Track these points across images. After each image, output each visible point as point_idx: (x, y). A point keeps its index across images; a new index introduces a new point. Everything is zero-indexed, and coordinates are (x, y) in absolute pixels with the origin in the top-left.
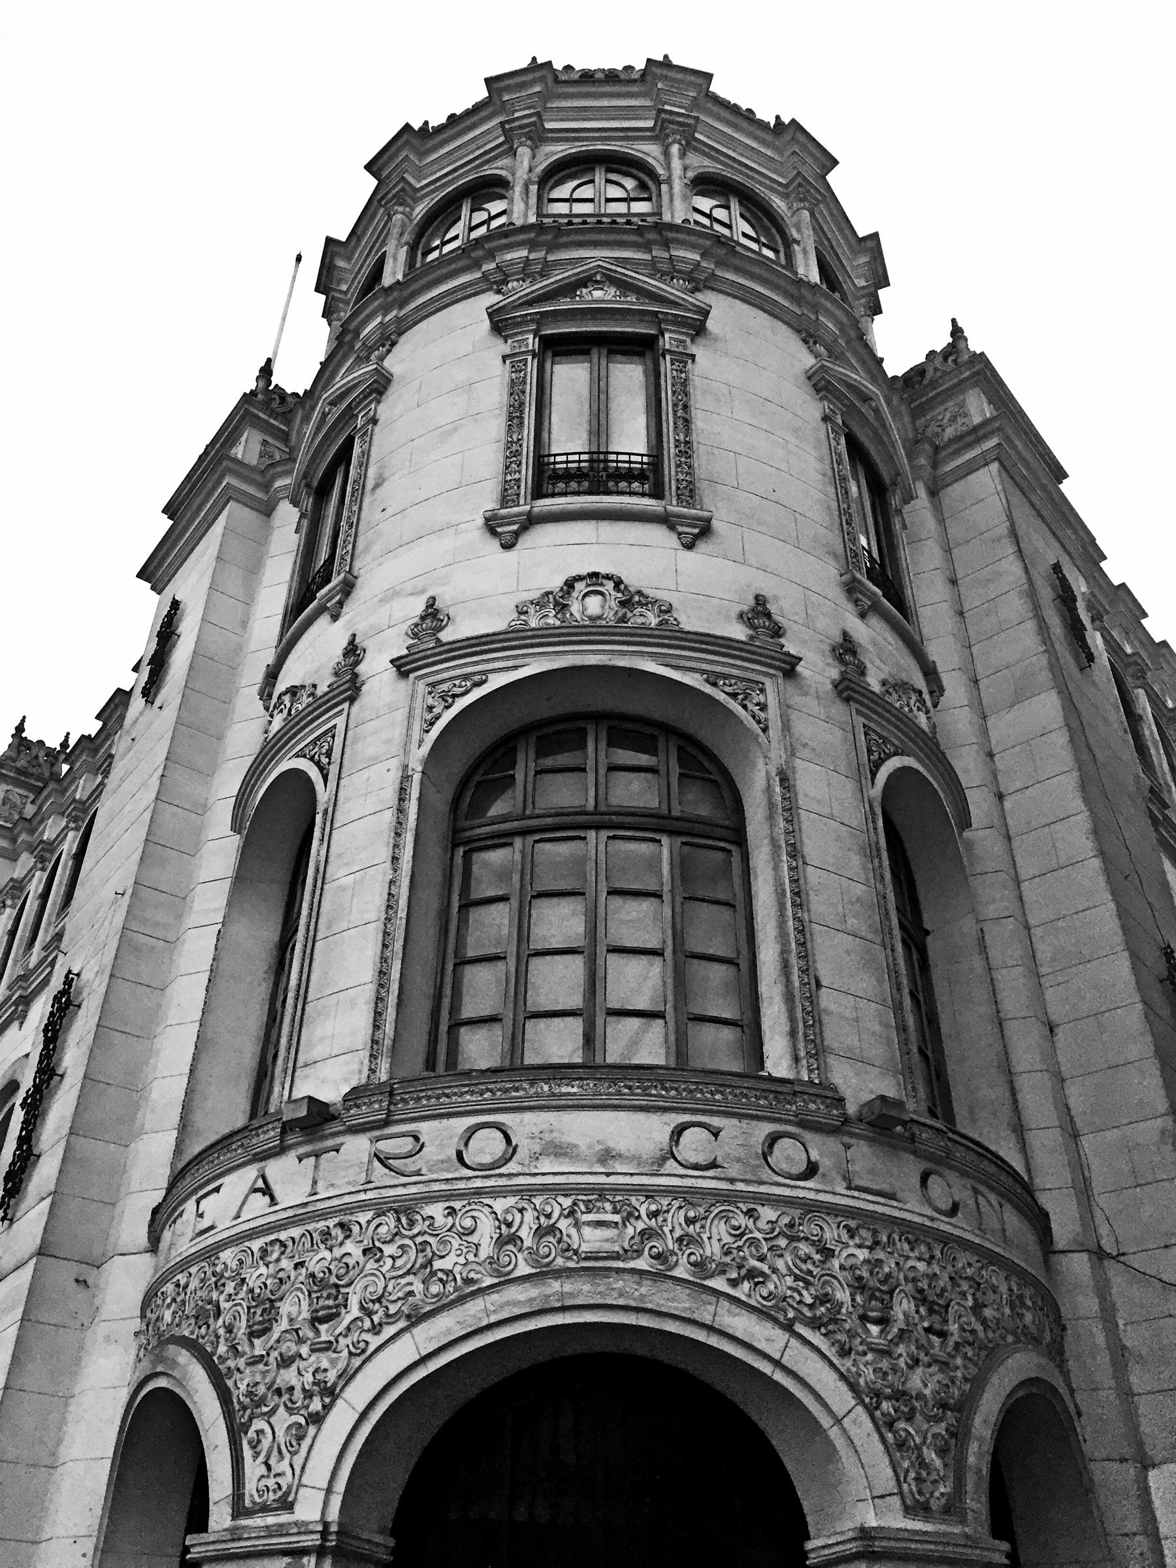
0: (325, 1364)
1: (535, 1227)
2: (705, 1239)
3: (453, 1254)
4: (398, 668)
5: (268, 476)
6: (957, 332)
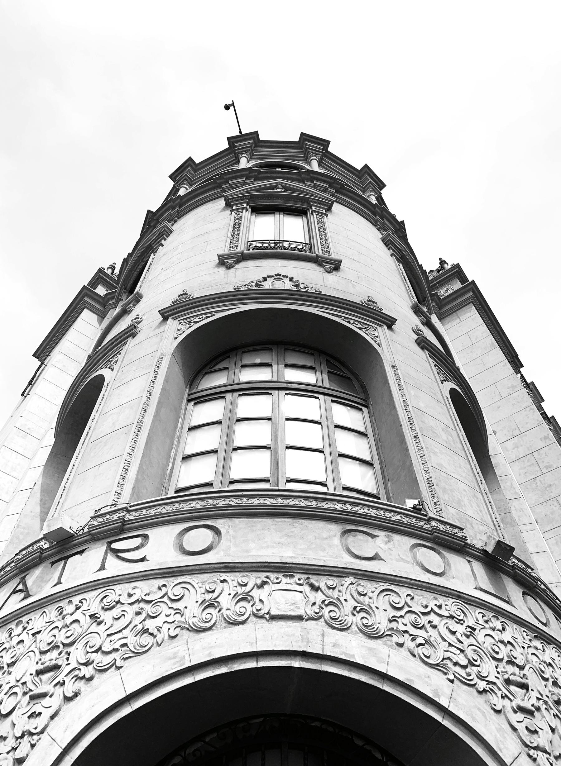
0: (37, 708)
1: (233, 593)
2: (375, 609)
3: (163, 615)
4: (162, 315)
5: (106, 299)
6: (442, 262)
